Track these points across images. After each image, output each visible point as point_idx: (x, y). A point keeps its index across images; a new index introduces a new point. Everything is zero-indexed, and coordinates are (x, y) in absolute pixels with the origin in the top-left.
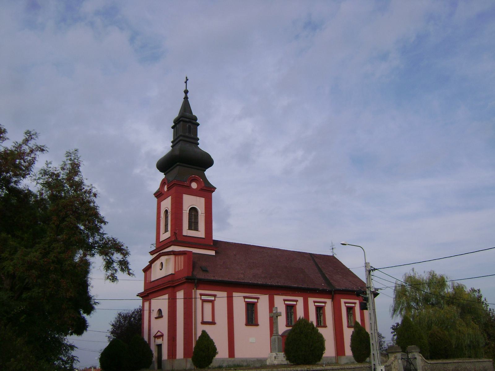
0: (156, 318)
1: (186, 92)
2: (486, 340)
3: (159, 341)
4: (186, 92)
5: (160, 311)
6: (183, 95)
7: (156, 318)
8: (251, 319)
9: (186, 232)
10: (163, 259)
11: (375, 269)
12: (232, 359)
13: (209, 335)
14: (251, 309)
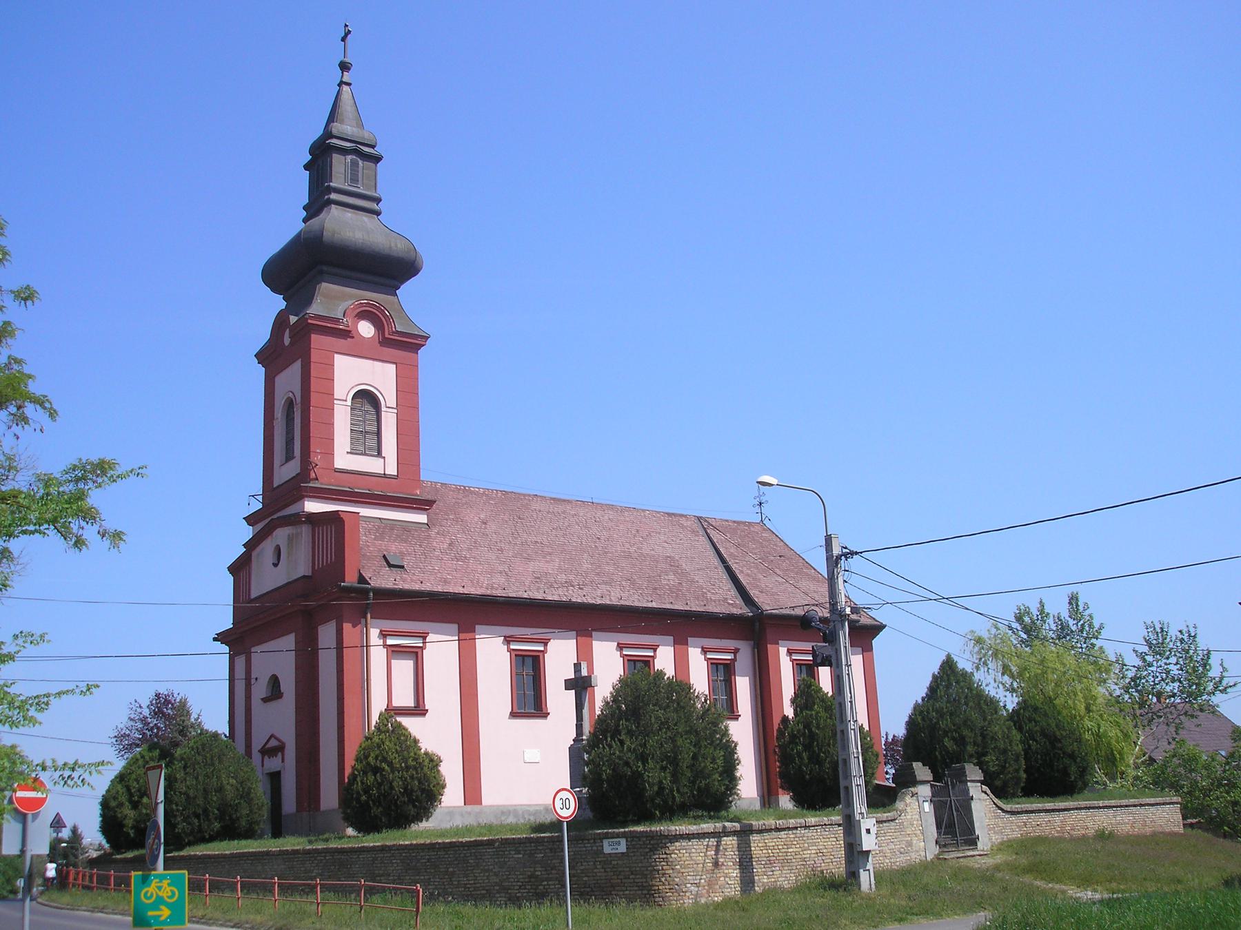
0: (265, 700)
3: (273, 764)
5: (275, 682)
7: (265, 700)
8: (530, 700)
10: (281, 535)
11: (853, 553)
12: (476, 808)
14: (529, 671)
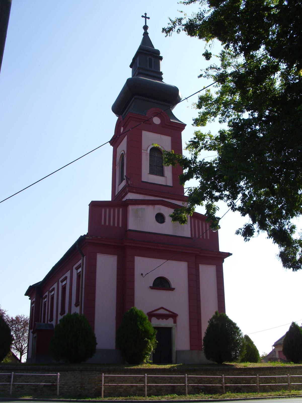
1: (146, 28)
2: (88, 390)
4: (146, 28)
6: (143, 31)
9: (147, 177)
13: (164, 320)
